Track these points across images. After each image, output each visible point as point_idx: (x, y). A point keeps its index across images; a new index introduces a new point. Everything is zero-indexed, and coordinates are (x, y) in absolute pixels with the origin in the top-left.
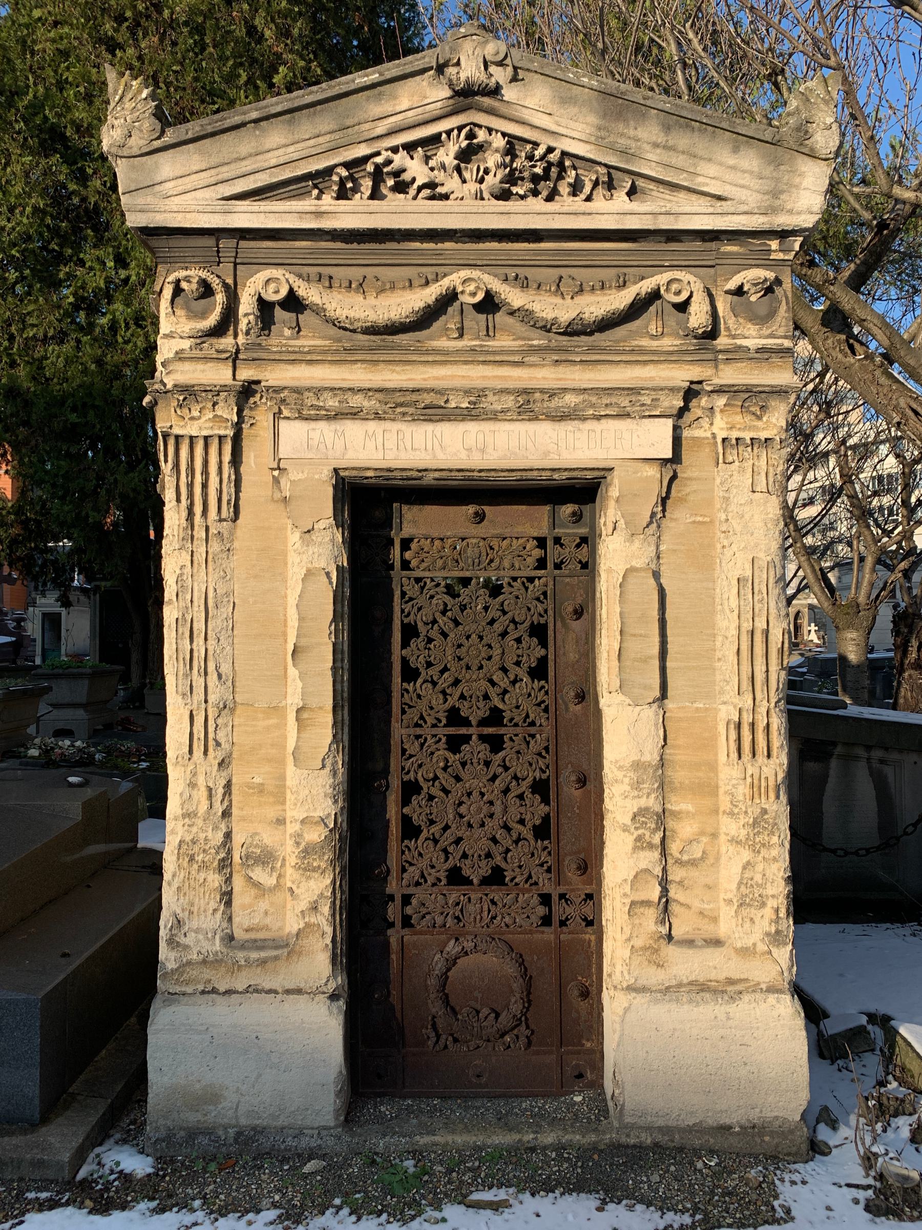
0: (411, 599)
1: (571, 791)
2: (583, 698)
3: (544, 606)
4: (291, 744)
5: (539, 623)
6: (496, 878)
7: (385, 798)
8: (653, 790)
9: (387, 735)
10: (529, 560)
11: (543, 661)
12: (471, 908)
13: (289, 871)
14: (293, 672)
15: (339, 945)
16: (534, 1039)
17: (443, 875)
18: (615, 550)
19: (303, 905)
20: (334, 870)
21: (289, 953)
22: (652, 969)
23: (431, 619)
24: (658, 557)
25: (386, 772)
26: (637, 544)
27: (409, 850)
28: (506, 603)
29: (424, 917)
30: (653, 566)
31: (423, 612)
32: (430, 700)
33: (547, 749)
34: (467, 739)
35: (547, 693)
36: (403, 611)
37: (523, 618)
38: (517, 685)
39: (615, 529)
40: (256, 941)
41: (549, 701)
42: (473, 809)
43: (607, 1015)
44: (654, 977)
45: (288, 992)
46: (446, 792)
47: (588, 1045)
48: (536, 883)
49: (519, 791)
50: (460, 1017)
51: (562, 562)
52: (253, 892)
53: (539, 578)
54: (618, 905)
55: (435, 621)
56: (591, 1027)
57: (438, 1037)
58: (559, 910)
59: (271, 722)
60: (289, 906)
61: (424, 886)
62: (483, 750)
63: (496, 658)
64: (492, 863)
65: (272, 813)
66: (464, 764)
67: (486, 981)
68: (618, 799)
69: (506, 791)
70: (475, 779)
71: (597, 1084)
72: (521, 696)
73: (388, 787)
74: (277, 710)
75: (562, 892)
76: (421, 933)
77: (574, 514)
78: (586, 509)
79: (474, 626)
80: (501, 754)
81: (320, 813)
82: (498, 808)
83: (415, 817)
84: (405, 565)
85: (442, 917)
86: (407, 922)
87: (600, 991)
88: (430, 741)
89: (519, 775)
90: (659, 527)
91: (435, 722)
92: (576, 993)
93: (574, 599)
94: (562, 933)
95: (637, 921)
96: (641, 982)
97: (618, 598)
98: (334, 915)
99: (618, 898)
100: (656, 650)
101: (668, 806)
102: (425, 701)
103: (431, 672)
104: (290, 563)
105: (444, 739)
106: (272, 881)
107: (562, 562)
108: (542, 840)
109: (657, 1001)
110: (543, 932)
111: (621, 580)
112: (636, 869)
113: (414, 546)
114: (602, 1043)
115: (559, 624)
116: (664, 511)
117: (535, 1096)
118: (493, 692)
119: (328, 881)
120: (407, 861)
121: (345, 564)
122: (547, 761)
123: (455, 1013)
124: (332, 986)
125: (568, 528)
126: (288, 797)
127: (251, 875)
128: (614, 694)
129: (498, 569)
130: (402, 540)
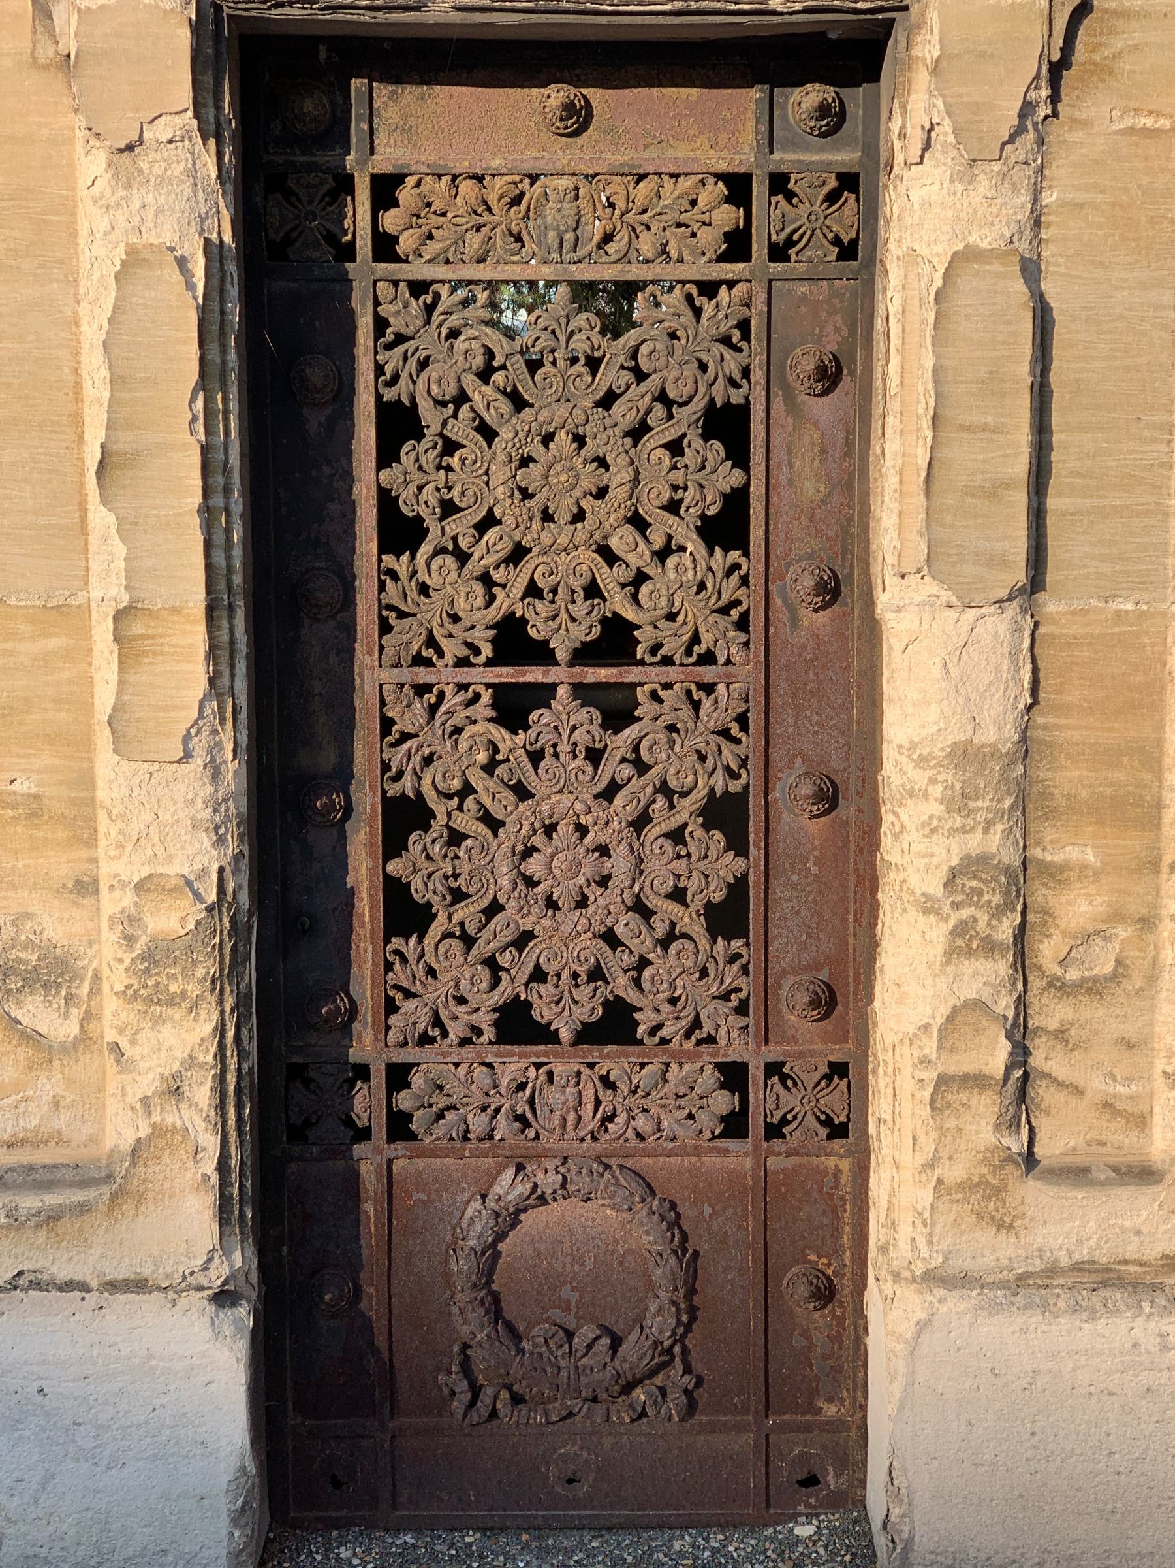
0: (400, 339)
1: (796, 823)
2: (836, 593)
3: (743, 358)
4: (104, 699)
5: (727, 404)
6: (615, 1025)
7: (343, 837)
8: (1000, 814)
9: (347, 685)
10: (704, 234)
11: (737, 500)
12: (553, 1096)
13: (111, 1005)
14: (101, 518)
15: (235, 1177)
16: (702, 1395)
17: (485, 1020)
18: (926, 204)
19: (147, 1083)
20: (221, 1001)
21: (114, 1196)
22: (985, 1236)
23: (451, 390)
24: (1037, 224)
25: (344, 775)
26: (984, 186)
27: (404, 960)
28: (644, 350)
29: (440, 1116)
30: (1023, 246)
31: (433, 371)
32: (453, 600)
33: (742, 720)
34: (543, 694)
35: (745, 581)
36: (379, 369)
37: (688, 390)
38: (672, 561)
39: (927, 146)
40: (32, 1168)
41: (752, 600)
42: (561, 866)
43: (877, 1343)
44: (990, 1251)
45: (113, 1286)
46: (493, 824)
47: (831, 1410)
48: (711, 1040)
49: (674, 823)
50: (526, 1345)
51: (790, 243)
52: (23, 1053)
53: (731, 284)
54: (906, 1084)
55: (462, 398)
56: (839, 1370)
57: (476, 1391)
58: (765, 1099)
59: (53, 643)
60: (111, 1088)
61: (441, 1045)
62: (585, 723)
63: (618, 494)
64: (605, 992)
65: (63, 865)
66: (536, 757)
67: (590, 1264)
68: (913, 836)
69: (641, 822)
70: (562, 791)
71: (851, 1499)
72: (679, 591)
73: (348, 810)
74: (67, 616)
75: (772, 1057)
76: (434, 1153)
77: (823, 110)
78: (856, 97)
79: (562, 411)
80: (631, 732)
81: (180, 867)
82: (619, 864)
83: (416, 883)
84: (385, 248)
85: (485, 1118)
86: (400, 1127)
87: (860, 1286)
88: (453, 700)
89: (673, 783)
90: (1041, 141)
91: (463, 652)
92: (803, 1290)
93: (819, 340)
94: (771, 1152)
95: (951, 1123)
96: (958, 1264)
97: (929, 332)
98: (222, 1107)
99: (907, 1071)
100: (1021, 466)
101: (1036, 852)
102: (438, 601)
103: (453, 526)
104: (84, 232)
105: (486, 696)
106: (70, 1029)
107: (790, 243)
108: (726, 551)
109: (994, 1308)
110: (726, 1152)
111: (938, 283)
112: (953, 1001)
113: (405, 194)
114: (863, 1408)
115: (778, 404)
116: (1055, 98)
117: (704, 1525)
118: (610, 579)
119: (206, 1026)
120: (398, 987)
121: (228, 238)
122: (741, 750)
123: (515, 1335)
124: (219, 1273)
125: (807, 148)
126: (102, 829)
127: (17, 1013)
128: (912, 580)
129: (624, 258)
130: (374, 177)
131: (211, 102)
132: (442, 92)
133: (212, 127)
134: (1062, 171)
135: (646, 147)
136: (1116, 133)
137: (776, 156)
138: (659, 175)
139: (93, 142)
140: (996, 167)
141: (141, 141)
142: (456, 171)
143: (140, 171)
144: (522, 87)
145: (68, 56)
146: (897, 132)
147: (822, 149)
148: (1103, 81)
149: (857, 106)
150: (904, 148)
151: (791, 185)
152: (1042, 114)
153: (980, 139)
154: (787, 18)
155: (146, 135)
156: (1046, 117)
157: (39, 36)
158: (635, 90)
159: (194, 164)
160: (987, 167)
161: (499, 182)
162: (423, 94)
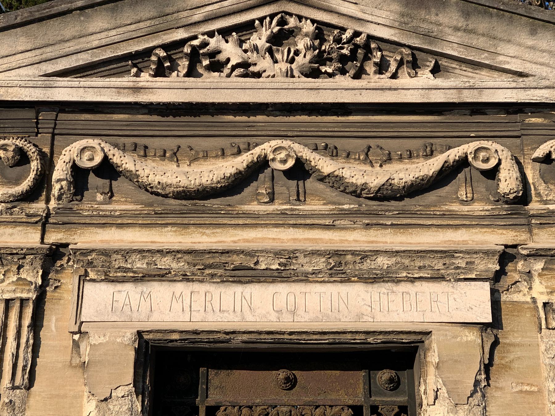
39: (436, 398)
77: (391, 380)
78: (404, 375)
90: (484, 396)
116: (488, 378)
125: (385, 395)
131: (141, 380)
132: (237, 373)
133: (141, 390)
134: (494, 408)
135: (319, 394)
136: (515, 392)
137: (373, 398)
138: (325, 406)
139: (91, 397)
140: (466, 407)
141: (111, 397)
142: (241, 404)
143: (109, 409)
144: (269, 370)
145: (85, 362)
146: (423, 391)
147: (391, 396)
148: (507, 371)
149: (405, 378)
150: (427, 398)
151: (379, 410)
152: (483, 385)
153: (459, 395)
154: (375, 345)
155: (113, 394)
156: (485, 386)
157: (74, 355)
158: (314, 372)
159: (132, 406)
160: (462, 407)
161: (259, 409)
162: (229, 374)
